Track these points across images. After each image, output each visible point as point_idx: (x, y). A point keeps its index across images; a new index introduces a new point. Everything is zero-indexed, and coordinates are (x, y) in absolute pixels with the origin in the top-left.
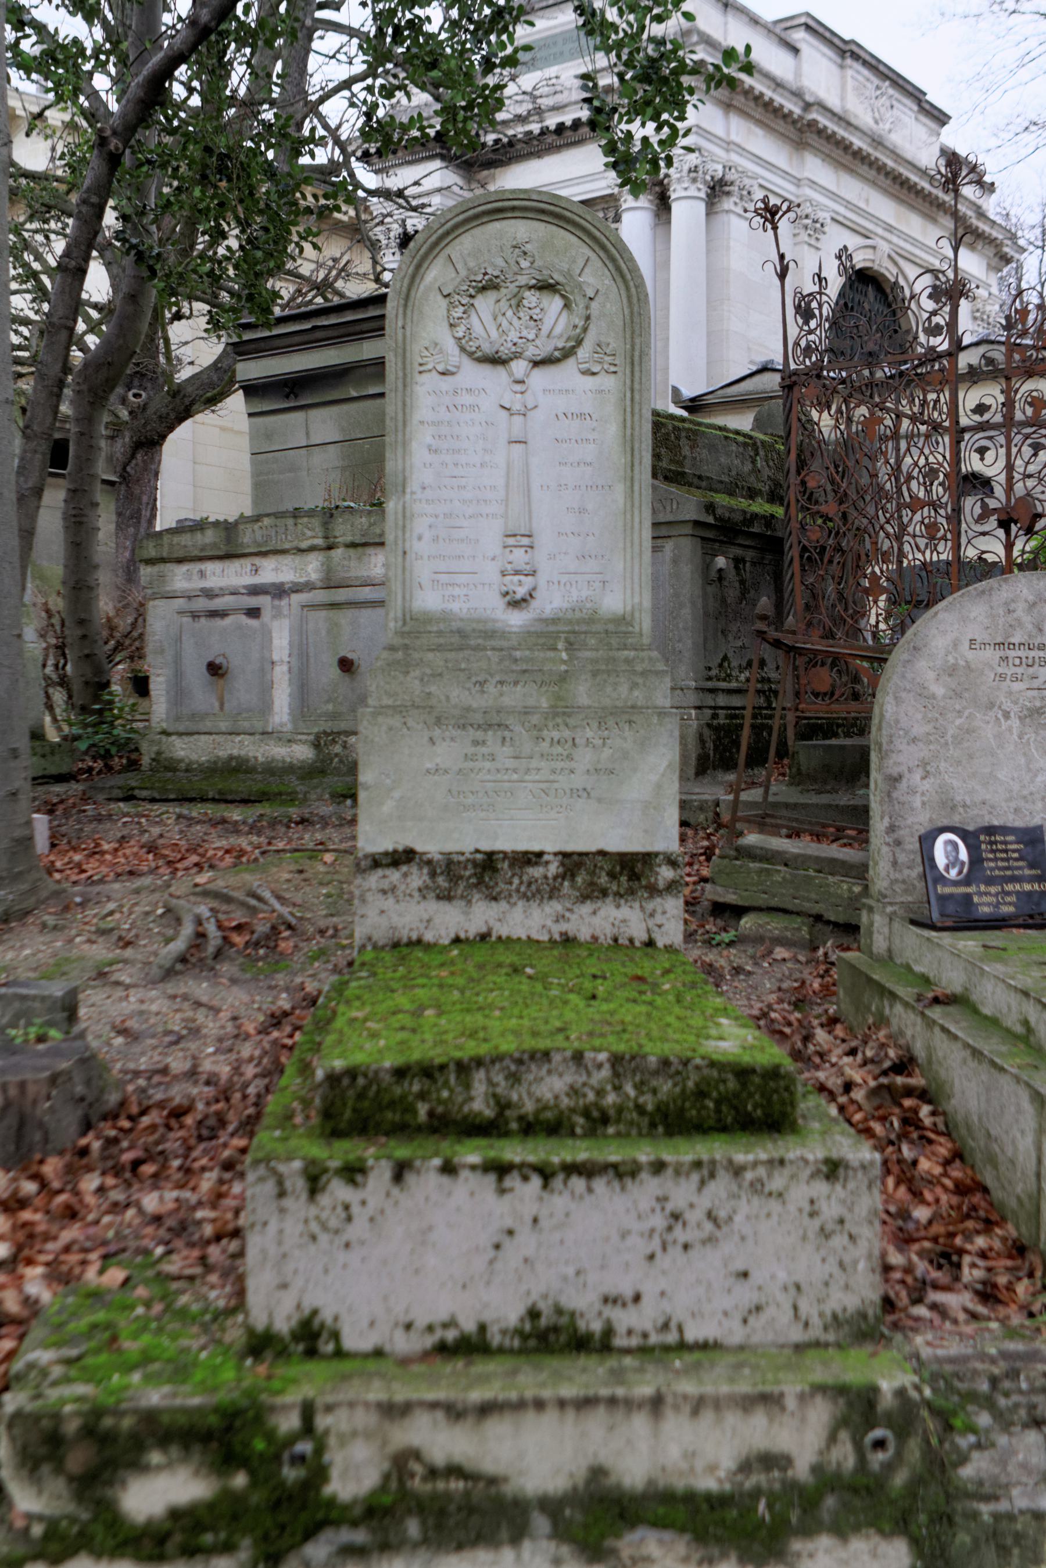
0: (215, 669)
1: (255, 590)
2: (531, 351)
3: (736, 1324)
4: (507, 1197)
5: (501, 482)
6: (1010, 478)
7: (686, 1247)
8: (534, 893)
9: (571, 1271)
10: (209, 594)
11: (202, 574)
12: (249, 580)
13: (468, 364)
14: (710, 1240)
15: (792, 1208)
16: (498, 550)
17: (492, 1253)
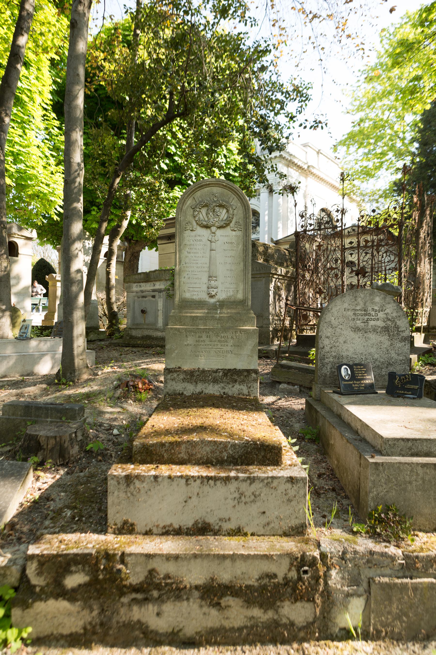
0: (143, 312)
1: (154, 291)
2: (217, 224)
3: (261, 528)
4: (189, 486)
6: (359, 262)
7: (245, 503)
8: (215, 381)
9: (209, 510)
10: (142, 291)
11: (140, 286)
12: (152, 288)
13: (199, 228)
14: (254, 501)
15: (279, 492)
16: (207, 281)
17: (184, 504)
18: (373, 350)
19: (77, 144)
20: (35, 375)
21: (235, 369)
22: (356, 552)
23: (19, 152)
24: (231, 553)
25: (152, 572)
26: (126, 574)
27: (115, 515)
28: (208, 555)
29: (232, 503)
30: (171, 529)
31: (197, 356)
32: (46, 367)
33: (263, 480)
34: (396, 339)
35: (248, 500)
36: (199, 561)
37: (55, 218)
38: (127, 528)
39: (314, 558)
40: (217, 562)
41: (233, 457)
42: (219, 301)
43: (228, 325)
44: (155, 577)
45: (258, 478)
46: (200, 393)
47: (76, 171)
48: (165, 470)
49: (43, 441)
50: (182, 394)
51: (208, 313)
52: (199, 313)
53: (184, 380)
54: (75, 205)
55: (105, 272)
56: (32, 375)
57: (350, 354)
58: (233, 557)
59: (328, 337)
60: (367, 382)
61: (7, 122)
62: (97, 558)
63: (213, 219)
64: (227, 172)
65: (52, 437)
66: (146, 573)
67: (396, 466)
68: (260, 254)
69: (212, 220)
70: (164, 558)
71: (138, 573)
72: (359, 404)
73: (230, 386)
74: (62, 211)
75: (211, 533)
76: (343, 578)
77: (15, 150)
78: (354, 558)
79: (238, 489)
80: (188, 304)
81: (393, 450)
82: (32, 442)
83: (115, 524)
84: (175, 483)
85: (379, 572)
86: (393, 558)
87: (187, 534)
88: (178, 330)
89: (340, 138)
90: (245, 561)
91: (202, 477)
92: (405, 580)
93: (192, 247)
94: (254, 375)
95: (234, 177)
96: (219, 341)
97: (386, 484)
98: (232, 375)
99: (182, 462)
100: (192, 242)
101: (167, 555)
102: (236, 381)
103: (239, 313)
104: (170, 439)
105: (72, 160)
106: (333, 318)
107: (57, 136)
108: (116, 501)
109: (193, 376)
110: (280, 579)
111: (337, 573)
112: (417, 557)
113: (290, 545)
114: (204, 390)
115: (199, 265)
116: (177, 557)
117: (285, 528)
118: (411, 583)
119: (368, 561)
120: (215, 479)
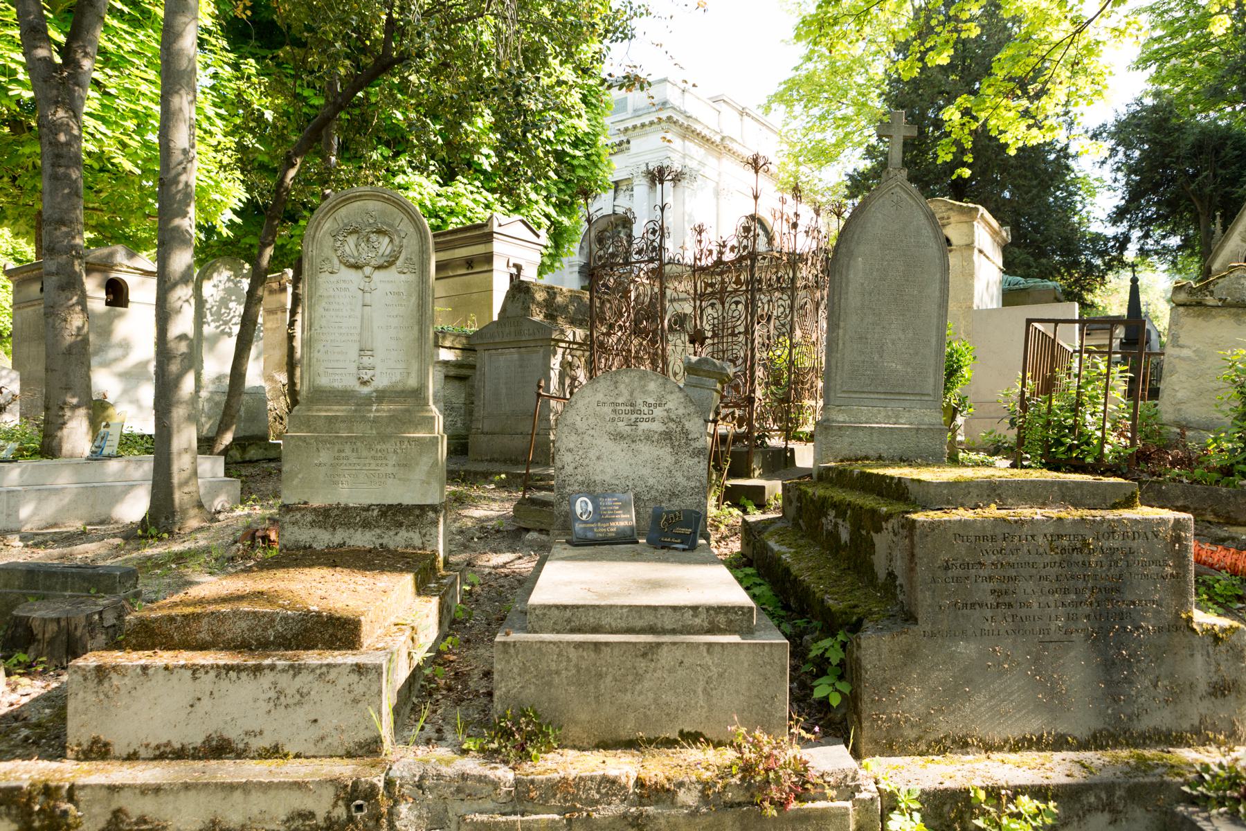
2: (373, 263)
5: (359, 325)
8: (366, 525)
9: (229, 718)
13: (343, 267)
14: (299, 703)
15: (339, 687)
18: (646, 472)
19: (181, 116)
20: (116, 522)
21: (400, 505)
22: (439, 776)
23: (149, 112)
24: (244, 780)
25: (117, 814)
26: (75, 817)
27: (78, 731)
28: (207, 785)
29: (265, 707)
30: (168, 750)
31: (336, 483)
32: (134, 508)
33: (313, 670)
34: (684, 453)
35: (290, 701)
36: (192, 793)
37: (225, 232)
38: (98, 751)
39: (373, 787)
40: (221, 795)
41: (284, 637)
42: (376, 391)
43: (389, 430)
44: (122, 822)
45: (307, 667)
46: (341, 545)
47: (181, 163)
48: (165, 658)
49: (36, 627)
50: (310, 547)
51: (356, 411)
52: (339, 410)
53: (313, 524)
54: (177, 222)
55: (286, 335)
56: (109, 523)
57: (607, 478)
58: (246, 787)
59: (570, 450)
60: (622, 524)
61: (86, 68)
62: (30, 793)
63: (366, 254)
64: (559, 148)
65: (52, 620)
66: (109, 816)
67: (535, 647)
68: (538, 304)
69: (364, 255)
70: (137, 791)
71: (95, 816)
72: (590, 560)
73: (392, 533)
74: (238, 221)
75: (233, 755)
76: (419, 817)
77: (139, 108)
78: (437, 786)
79: (275, 684)
80: (322, 396)
81: (542, 623)
82: (20, 630)
83: (79, 745)
84: (175, 677)
85: (475, 806)
86: (495, 785)
87: (194, 757)
88: (303, 439)
89: (774, 89)
90: (265, 793)
91: (218, 666)
92: (513, 818)
93: (332, 300)
94: (431, 514)
95: (574, 157)
96: (374, 458)
97: (520, 675)
98: (394, 515)
99: (203, 647)
100: (332, 293)
101: (141, 786)
102: (401, 525)
103: (407, 411)
104: (190, 610)
105: (172, 145)
106: (578, 418)
107: (230, 81)
108: (81, 707)
109: (328, 517)
110: (320, 820)
111: (410, 809)
112: (532, 782)
113: (345, 770)
114: (348, 541)
115: (343, 331)
116: (157, 790)
117: (349, 744)
118: (522, 822)
119: (459, 790)
120: (238, 669)
